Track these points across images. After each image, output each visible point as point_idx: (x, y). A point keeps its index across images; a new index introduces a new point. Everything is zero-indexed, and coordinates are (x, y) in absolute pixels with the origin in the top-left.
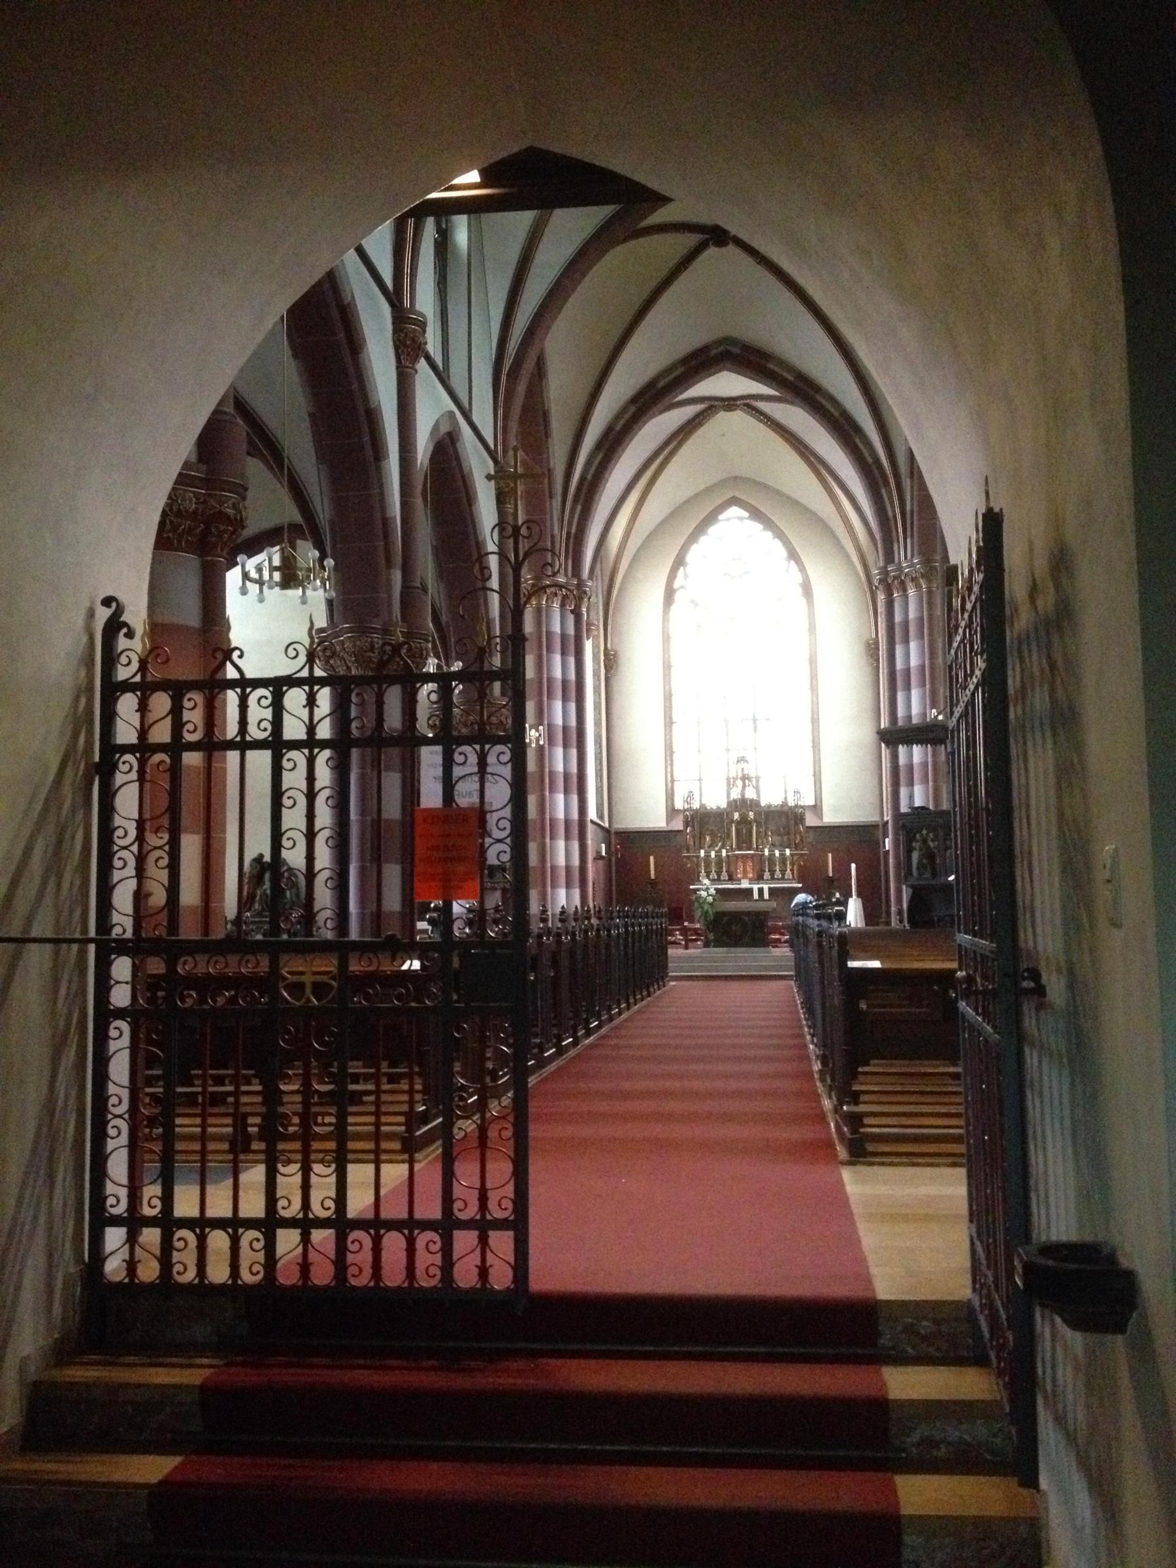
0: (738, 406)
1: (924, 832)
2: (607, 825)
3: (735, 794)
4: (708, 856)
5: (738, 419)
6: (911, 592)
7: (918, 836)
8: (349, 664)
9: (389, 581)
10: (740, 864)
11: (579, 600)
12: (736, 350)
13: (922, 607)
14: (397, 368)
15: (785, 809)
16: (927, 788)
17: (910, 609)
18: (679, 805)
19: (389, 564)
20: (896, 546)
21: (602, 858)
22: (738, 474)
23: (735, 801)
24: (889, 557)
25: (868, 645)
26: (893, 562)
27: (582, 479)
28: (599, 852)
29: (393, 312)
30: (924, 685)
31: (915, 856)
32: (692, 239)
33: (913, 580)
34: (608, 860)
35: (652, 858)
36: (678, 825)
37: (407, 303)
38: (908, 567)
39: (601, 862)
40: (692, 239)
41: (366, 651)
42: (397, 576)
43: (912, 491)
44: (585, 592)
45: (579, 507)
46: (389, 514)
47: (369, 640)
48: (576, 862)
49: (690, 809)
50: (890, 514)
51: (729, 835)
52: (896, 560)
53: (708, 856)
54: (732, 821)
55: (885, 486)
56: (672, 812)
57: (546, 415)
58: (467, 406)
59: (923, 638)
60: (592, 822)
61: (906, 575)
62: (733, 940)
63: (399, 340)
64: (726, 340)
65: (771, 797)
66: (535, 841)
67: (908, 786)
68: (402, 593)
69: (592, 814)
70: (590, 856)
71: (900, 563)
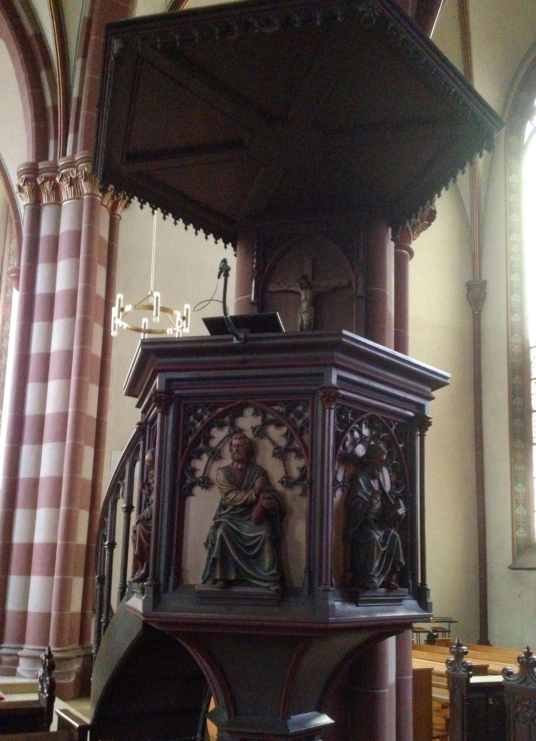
6: (68, 204)
13: (80, 218)
16: (63, 448)
17: (68, 145)
26: (46, 158)
30: (73, 314)
38: (65, 166)
43: (83, 74)
52: (51, 157)
55: (46, 68)
58: (372, 633)
59: (77, 255)
66: (78, 546)
67: (35, 443)
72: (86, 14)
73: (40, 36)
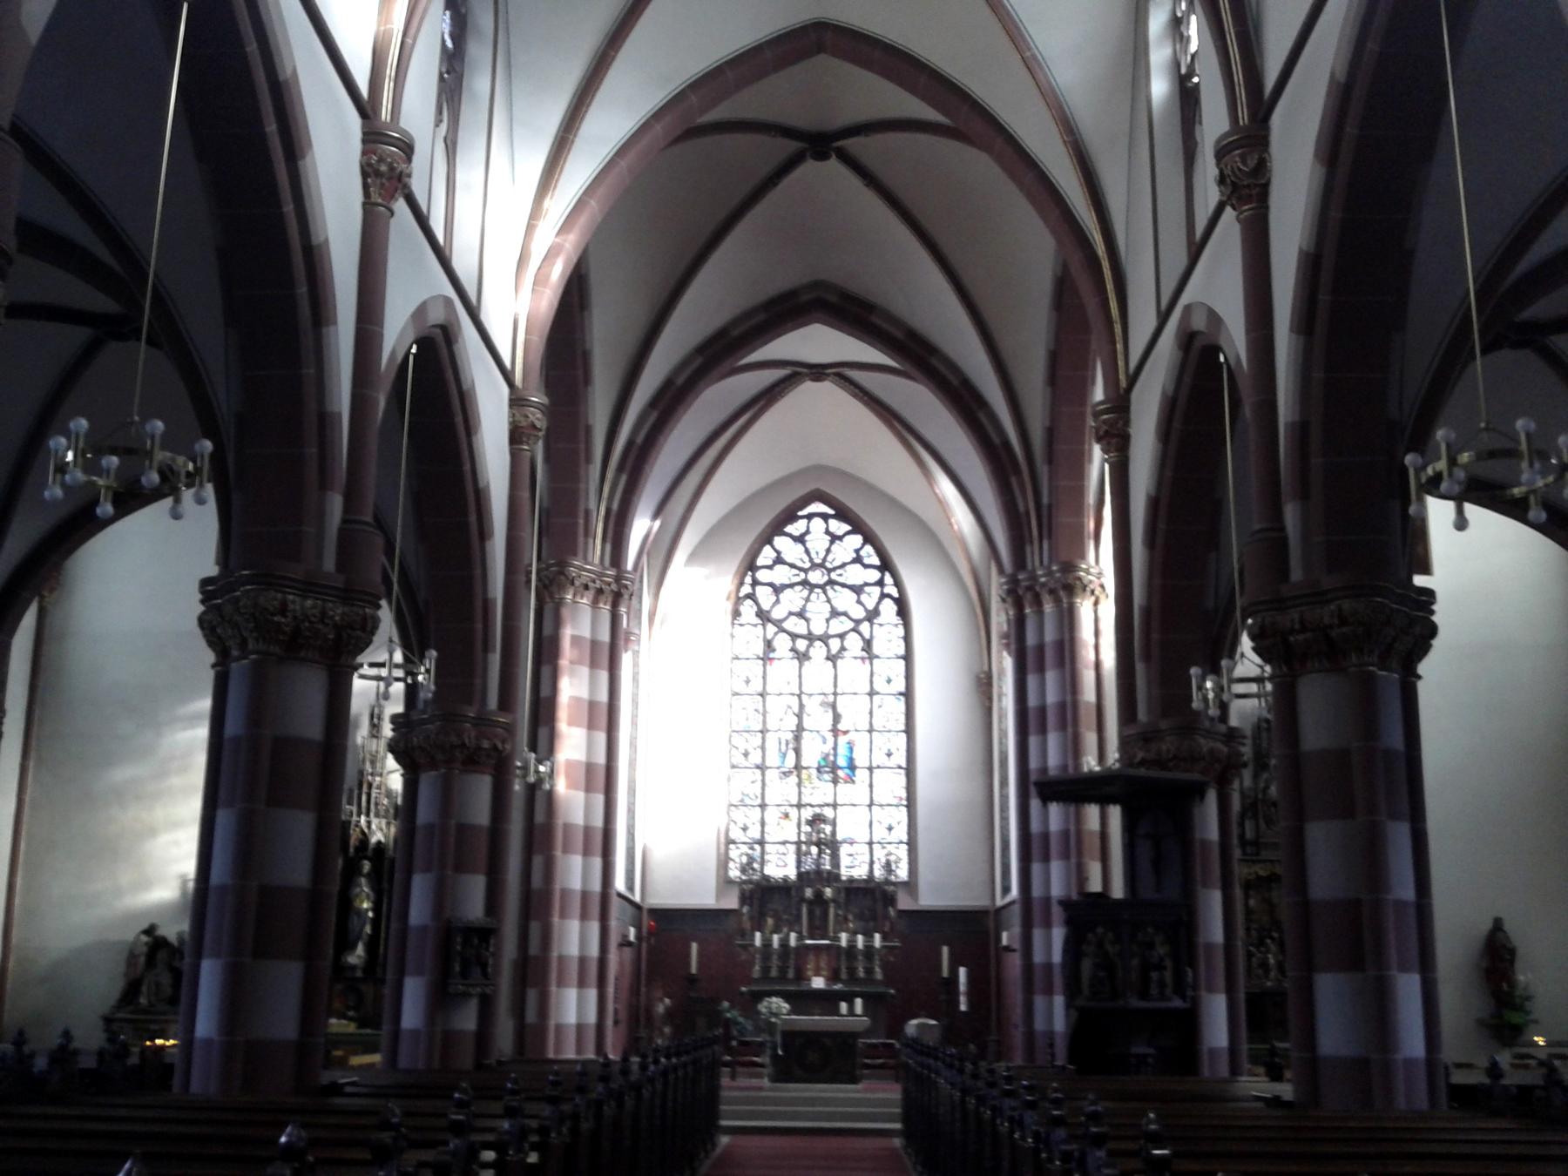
0: (828, 375)
1: (1100, 930)
2: (637, 898)
3: (808, 865)
4: (767, 944)
5: (827, 392)
6: (1048, 608)
7: (1090, 935)
8: (245, 634)
9: (321, 514)
10: (811, 957)
11: (617, 598)
12: (833, 298)
14: (364, 204)
15: (872, 885)
18: (734, 873)
19: (324, 485)
20: (1028, 549)
21: (629, 944)
22: (824, 462)
23: (808, 873)
24: (1020, 561)
25: (978, 679)
27: (630, 444)
28: (625, 936)
29: (364, 126)
31: (1087, 966)
32: (794, 146)
33: (1052, 592)
34: (636, 947)
35: (694, 946)
36: (731, 902)
37: (385, 114)
39: (627, 951)
40: (794, 146)
41: (273, 614)
42: (336, 505)
44: (626, 587)
45: (624, 478)
46: (332, 407)
47: (279, 596)
48: (594, 951)
49: (750, 882)
50: (1021, 508)
51: (798, 917)
53: (767, 944)
54: (803, 900)
56: (725, 882)
57: (586, 356)
60: (620, 895)
61: (1043, 585)
62: (813, 1074)
63: (369, 165)
64: (817, 285)
65: (854, 866)
68: (341, 531)
69: (620, 884)
70: (614, 940)
71: (1034, 570)
72: (1047, 424)
73: (1006, 444)
